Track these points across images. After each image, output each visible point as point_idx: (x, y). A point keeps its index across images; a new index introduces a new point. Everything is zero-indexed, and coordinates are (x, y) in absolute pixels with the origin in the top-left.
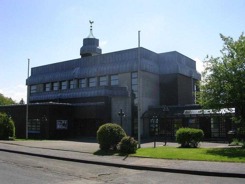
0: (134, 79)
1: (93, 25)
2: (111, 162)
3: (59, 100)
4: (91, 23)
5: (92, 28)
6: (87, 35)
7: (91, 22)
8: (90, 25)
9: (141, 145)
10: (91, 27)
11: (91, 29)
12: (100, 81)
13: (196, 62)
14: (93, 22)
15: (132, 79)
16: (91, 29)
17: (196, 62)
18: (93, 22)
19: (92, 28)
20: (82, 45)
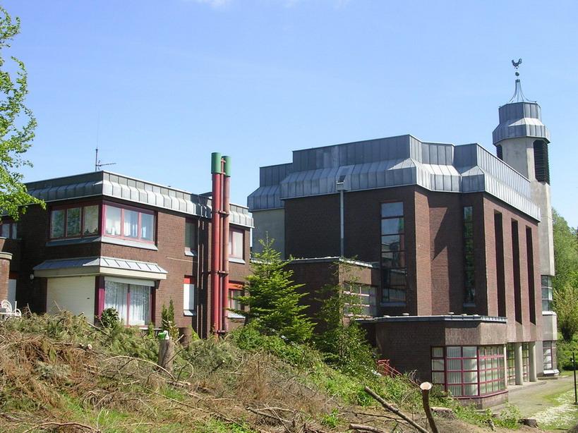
0: (443, 376)
1: (520, 69)
2: (239, 280)
3: (344, 194)
4: (516, 65)
5: (519, 78)
6: (508, 98)
7: (516, 61)
8: (514, 70)
9: (292, 162)
10: (517, 74)
11: (517, 81)
12: (383, 216)
13: (502, 105)
14: (520, 62)
15: (443, 370)
16: (517, 81)
17: (501, 109)
18: (520, 62)
19: (519, 78)
20: (496, 123)
